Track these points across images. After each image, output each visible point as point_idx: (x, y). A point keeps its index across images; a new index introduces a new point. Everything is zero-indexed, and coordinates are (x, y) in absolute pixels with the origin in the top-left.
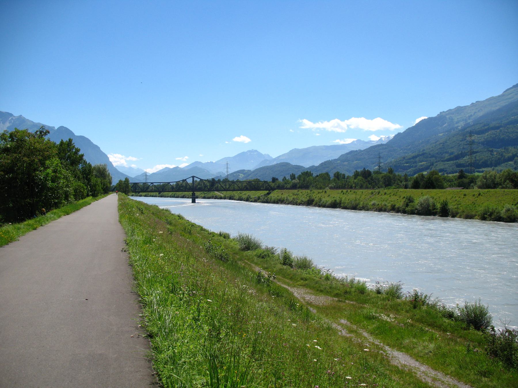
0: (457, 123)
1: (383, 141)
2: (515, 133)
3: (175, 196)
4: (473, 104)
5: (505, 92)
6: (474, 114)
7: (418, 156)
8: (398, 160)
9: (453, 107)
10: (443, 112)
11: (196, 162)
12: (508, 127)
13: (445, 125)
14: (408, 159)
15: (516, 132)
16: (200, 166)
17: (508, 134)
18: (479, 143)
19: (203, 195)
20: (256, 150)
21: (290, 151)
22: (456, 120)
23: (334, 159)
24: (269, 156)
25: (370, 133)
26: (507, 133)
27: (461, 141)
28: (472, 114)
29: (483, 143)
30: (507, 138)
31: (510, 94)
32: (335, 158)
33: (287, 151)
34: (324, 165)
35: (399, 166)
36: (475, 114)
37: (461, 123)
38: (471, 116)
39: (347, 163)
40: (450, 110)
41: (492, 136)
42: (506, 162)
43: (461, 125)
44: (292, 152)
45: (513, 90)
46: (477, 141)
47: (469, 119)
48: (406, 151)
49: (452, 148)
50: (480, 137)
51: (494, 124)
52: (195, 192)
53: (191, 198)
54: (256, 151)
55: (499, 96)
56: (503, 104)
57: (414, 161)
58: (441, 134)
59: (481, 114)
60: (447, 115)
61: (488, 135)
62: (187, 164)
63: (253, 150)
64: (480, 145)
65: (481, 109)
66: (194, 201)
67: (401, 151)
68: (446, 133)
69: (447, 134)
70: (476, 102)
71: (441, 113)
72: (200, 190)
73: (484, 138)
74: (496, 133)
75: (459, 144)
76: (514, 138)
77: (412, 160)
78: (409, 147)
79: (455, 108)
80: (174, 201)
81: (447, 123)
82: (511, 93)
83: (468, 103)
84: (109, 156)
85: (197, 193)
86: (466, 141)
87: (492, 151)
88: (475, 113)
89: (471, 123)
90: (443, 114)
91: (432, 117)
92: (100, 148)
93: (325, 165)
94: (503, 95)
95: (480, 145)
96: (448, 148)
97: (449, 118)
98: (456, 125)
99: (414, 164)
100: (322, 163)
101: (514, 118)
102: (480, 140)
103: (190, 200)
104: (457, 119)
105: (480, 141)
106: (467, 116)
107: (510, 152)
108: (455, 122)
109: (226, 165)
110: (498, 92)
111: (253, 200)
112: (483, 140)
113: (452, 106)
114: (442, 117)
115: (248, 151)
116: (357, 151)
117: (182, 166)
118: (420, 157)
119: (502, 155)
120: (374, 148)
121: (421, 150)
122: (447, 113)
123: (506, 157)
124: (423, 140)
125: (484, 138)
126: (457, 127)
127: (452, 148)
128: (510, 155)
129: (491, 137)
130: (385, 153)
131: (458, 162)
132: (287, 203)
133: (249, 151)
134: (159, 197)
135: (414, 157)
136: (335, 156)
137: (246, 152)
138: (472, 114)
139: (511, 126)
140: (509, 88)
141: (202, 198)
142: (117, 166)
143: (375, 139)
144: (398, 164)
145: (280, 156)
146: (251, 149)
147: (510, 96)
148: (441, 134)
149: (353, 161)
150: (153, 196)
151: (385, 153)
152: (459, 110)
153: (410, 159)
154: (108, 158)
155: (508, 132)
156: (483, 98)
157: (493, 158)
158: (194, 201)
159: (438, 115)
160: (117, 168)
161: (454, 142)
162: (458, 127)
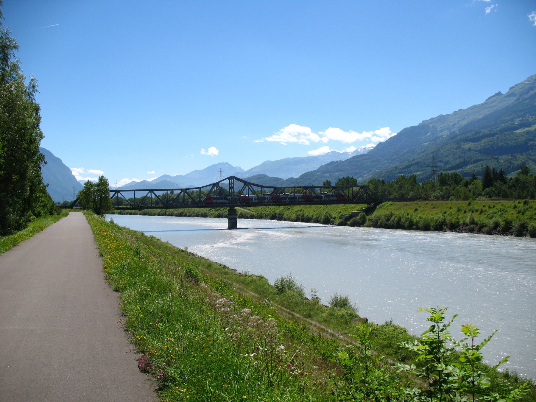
0: (440, 132)
1: (360, 152)
2: (514, 140)
3: (167, 213)
4: (455, 112)
5: (487, 100)
6: (458, 123)
7: (412, 165)
8: (389, 170)
9: (435, 116)
10: (426, 121)
11: (165, 176)
12: (505, 134)
13: (428, 134)
14: (401, 169)
15: (514, 139)
16: (168, 180)
17: (506, 141)
18: (476, 151)
19: (217, 213)
20: (227, 163)
21: (263, 163)
22: (439, 129)
23: (314, 171)
24: (240, 168)
25: (348, 145)
26: (505, 140)
27: (456, 149)
28: (456, 122)
29: (480, 151)
30: (506, 145)
31: (493, 102)
32: (314, 170)
33: (259, 163)
34: (305, 176)
35: (393, 176)
36: (460, 122)
37: (445, 132)
38: (455, 124)
39: (328, 174)
40: (432, 119)
41: (490, 144)
42: (516, 170)
43: (445, 134)
44: (264, 164)
45: (495, 98)
46: (474, 149)
47: (453, 128)
48: (390, 161)
49: (446, 156)
50: (476, 145)
51: (486, 131)
52: (236, 208)
53: (226, 217)
54: (227, 164)
55: (482, 104)
56: (487, 112)
57: (409, 170)
58: (427, 144)
59: (464, 123)
60: (430, 123)
61: (485, 142)
62: (155, 178)
63: (223, 162)
64: (477, 153)
65: (465, 118)
66: (233, 226)
67: (385, 161)
68: (432, 142)
69: (433, 144)
70: (459, 110)
71: (423, 121)
72: (246, 202)
73: (481, 146)
74: (493, 140)
75: (454, 153)
76: (514, 145)
77: (406, 170)
78: (394, 157)
79: (437, 117)
80: (176, 223)
81: (430, 132)
82: (495, 101)
83: (451, 112)
84: (71, 169)
85: (240, 210)
86: (461, 149)
87: (497, 159)
88: (459, 121)
89: (456, 132)
90: (425, 123)
91: (415, 125)
92: (61, 161)
93: (306, 176)
94: (486, 103)
95: (477, 153)
96: (442, 157)
97: (432, 127)
98: (440, 134)
99: (409, 173)
100: (303, 175)
101: (505, 126)
102: (477, 147)
103: (224, 223)
104: (441, 127)
105: (477, 148)
106: (451, 124)
107: (518, 160)
108: (438, 131)
109: (219, 173)
110: (480, 100)
111: (338, 221)
112: (479, 148)
113: (435, 115)
114: (424, 127)
115: (218, 163)
116: (337, 162)
117: (150, 180)
118: (414, 166)
119: (510, 163)
120: (356, 159)
121: (410, 160)
122: (430, 121)
123: (516, 164)
124: (408, 150)
125: (481, 146)
126: (442, 136)
127: (446, 156)
128: (520, 162)
129: (489, 144)
130: (368, 164)
131: (463, 171)
132: (367, 223)
133: (220, 164)
134: (140, 214)
135: (407, 167)
136: (314, 167)
137: (217, 165)
138: (456, 122)
139: (507, 133)
140: (491, 95)
141: (215, 217)
142: (80, 181)
143: (351, 150)
144: (391, 174)
145: (252, 169)
146: (221, 162)
147: (493, 104)
148: (427, 144)
149: (335, 172)
150: (131, 214)
151: (368, 164)
152: (442, 118)
153: (403, 169)
154: (71, 172)
155: (506, 140)
156: (465, 106)
157: (501, 166)
158: (233, 226)
159: (420, 123)
160: (80, 182)
161: (448, 150)
162: (442, 136)
